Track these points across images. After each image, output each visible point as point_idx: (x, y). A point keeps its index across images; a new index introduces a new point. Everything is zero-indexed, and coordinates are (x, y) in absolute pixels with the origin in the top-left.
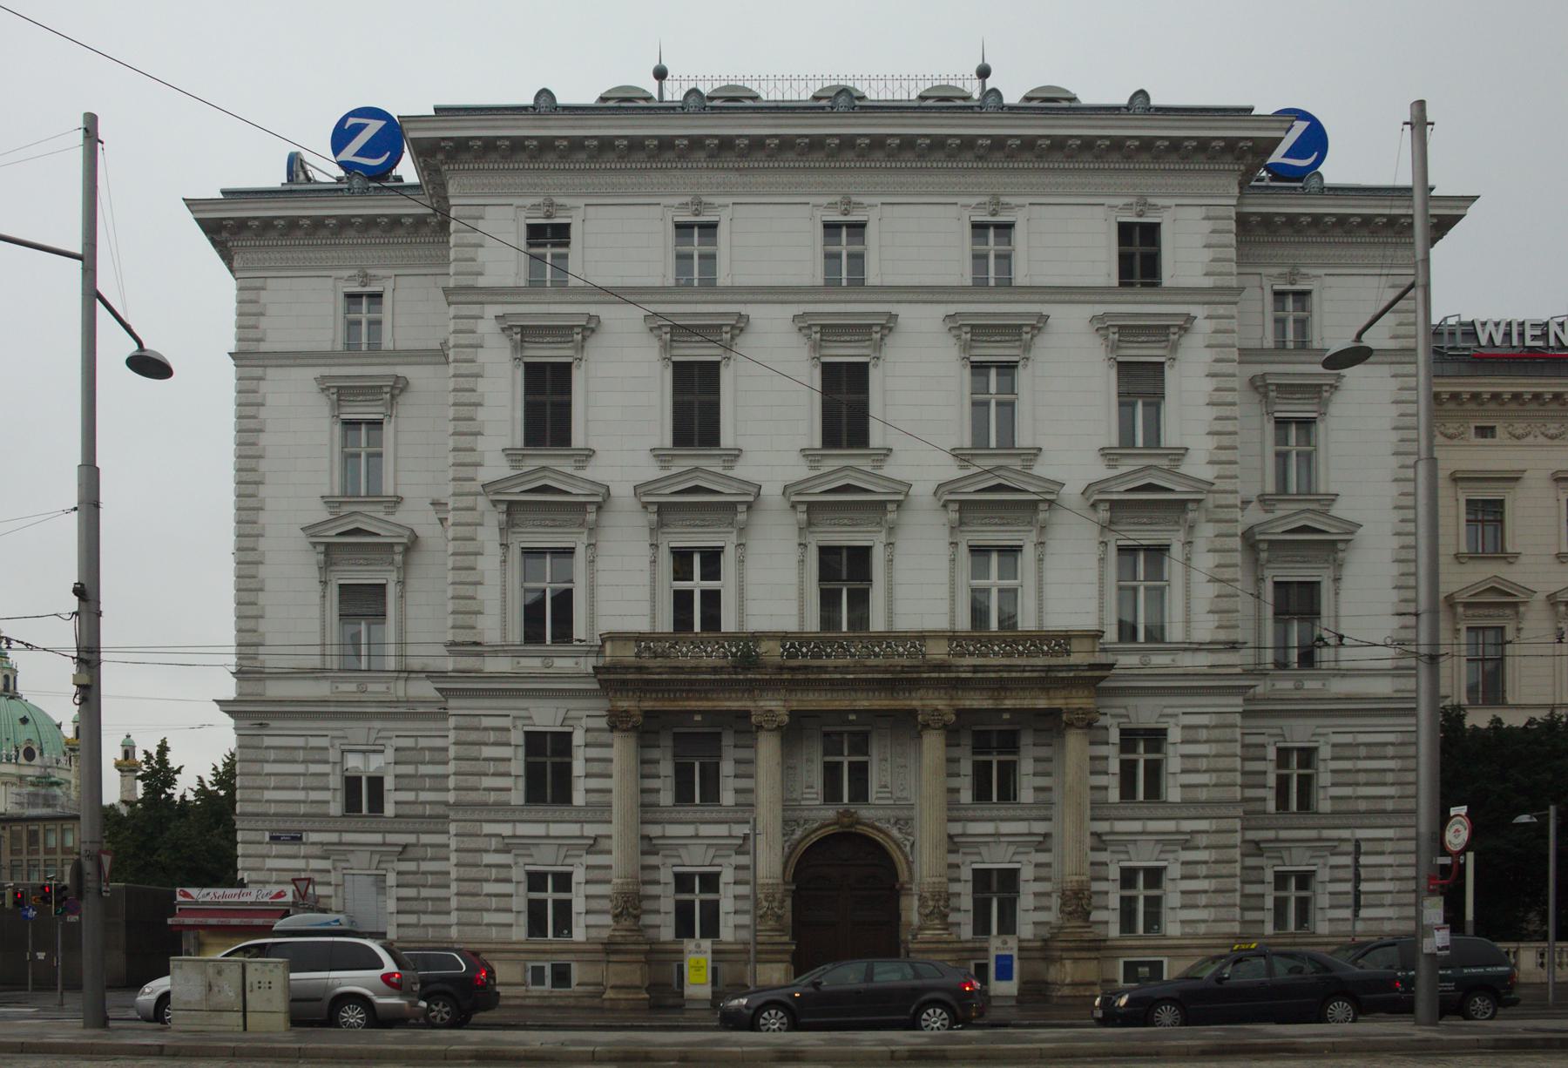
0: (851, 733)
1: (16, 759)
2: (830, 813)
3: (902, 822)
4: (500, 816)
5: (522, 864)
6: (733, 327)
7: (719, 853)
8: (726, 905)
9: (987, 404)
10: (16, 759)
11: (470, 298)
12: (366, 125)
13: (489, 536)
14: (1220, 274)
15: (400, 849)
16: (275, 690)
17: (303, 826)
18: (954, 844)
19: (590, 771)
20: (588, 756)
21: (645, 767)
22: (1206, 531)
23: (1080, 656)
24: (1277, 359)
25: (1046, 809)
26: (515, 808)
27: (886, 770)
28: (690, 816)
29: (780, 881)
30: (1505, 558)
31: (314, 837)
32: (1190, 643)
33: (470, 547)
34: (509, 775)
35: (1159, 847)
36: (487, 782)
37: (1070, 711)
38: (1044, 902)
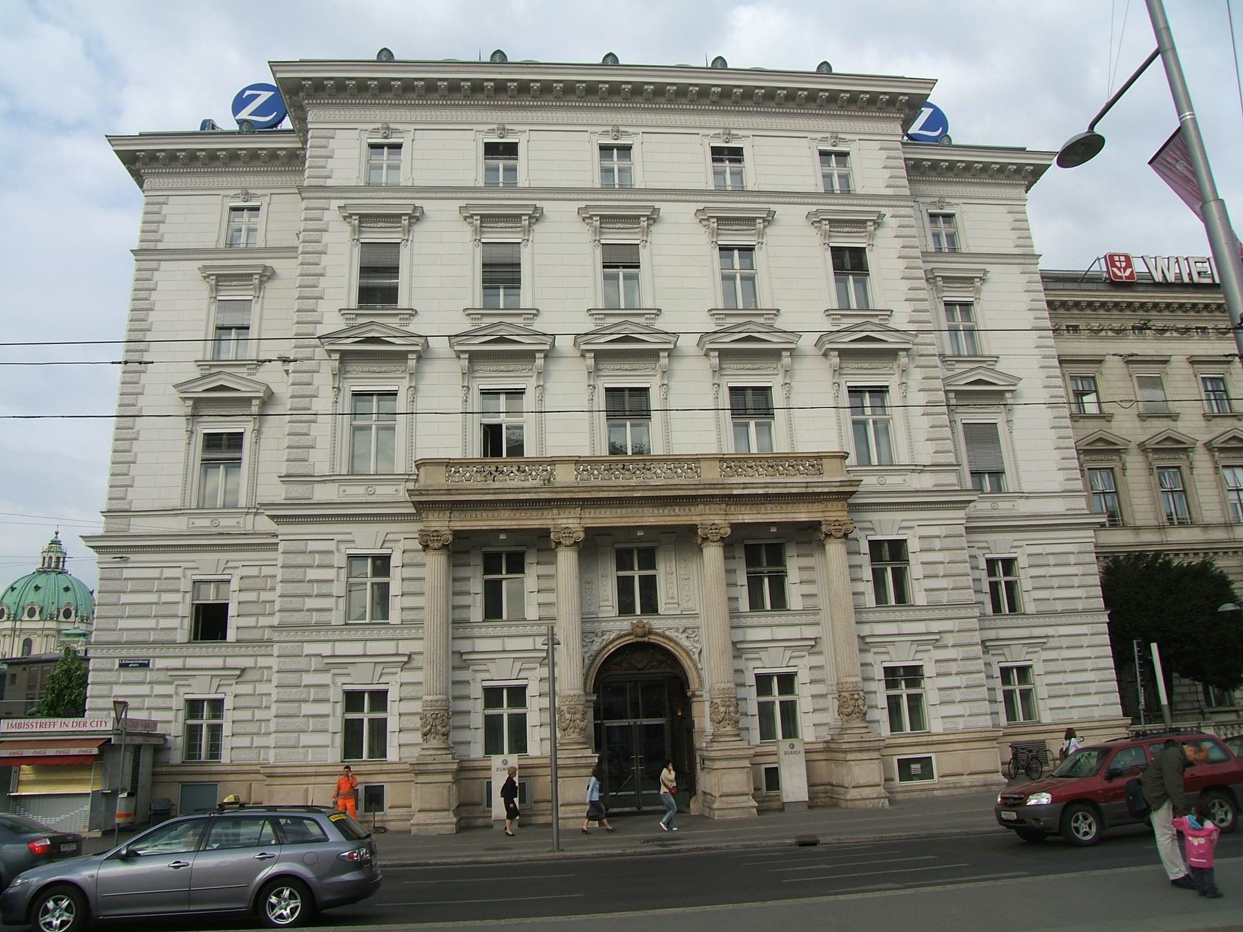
0: (639, 550)
1: (57, 618)
2: (625, 624)
3: (689, 631)
4: (322, 636)
5: (340, 684)
6: (531, 217)
7: (525, 666)
8: (533, 718)
9: (733, 278)
10: (57, 618)
11: (319, 195)
12: (259, 95)
13: (324, 380)
14: (897, 187)
15: (238, 673)
16: (139, 526)
17: (151, 653)
18: (738, 650)
19: (405, 590)
20: (405, 576)
21: (456, 584)
22: (916, 375)
23: (832, 476)
24: (938, 259)
25: (813, 614)
26: (335, 628)
27: (672, 583)
28: (498, 631)
29: (582, 692)
30: (1104, 417)
31: (160, 663)
32: (916, 465)
33: (307, 390)
34: (330, 596)
35: (915, 647)
36: (310, 603)
37: (829, 523)
38: (821, 703)
